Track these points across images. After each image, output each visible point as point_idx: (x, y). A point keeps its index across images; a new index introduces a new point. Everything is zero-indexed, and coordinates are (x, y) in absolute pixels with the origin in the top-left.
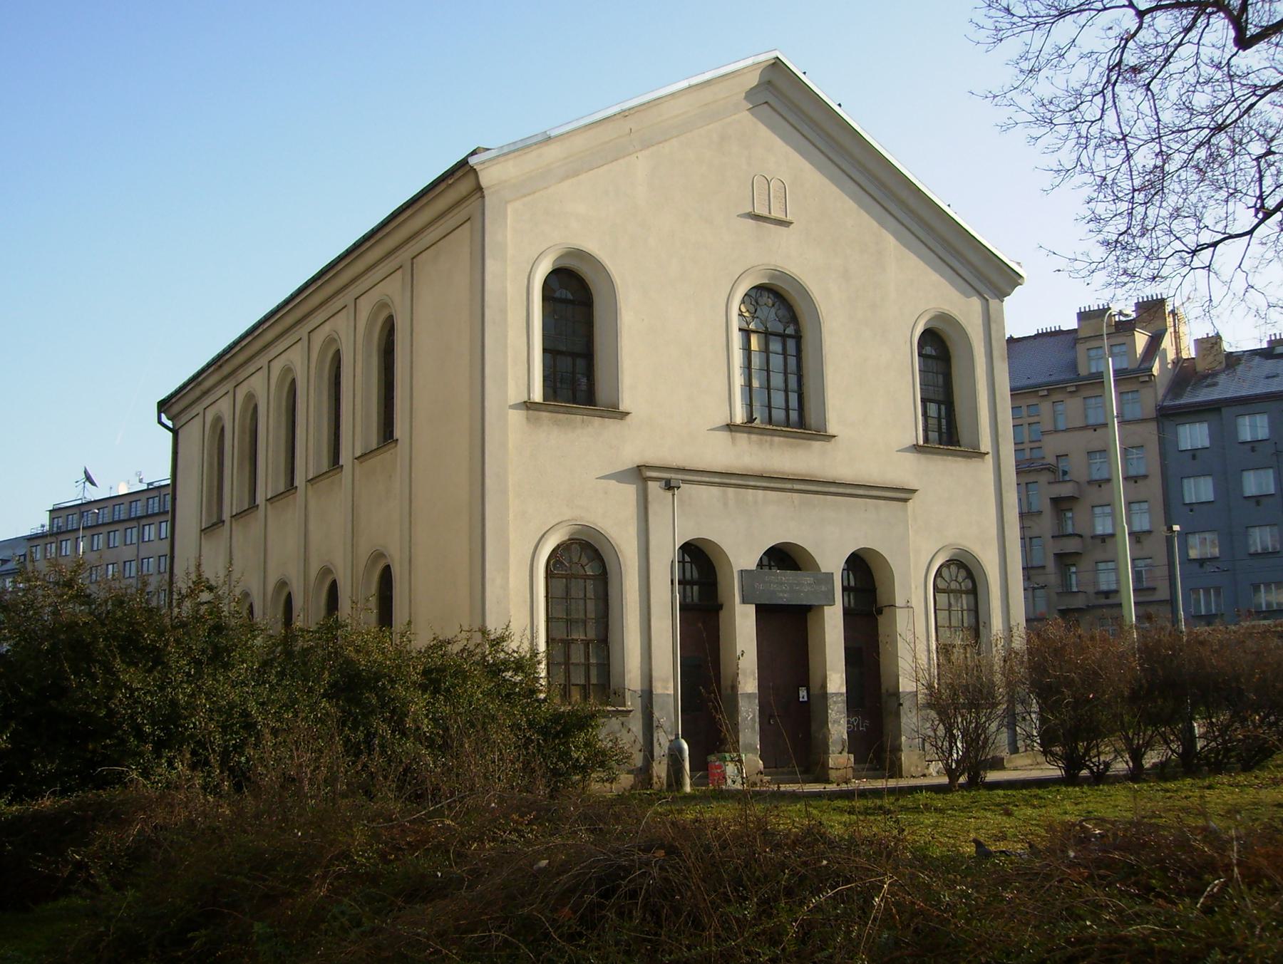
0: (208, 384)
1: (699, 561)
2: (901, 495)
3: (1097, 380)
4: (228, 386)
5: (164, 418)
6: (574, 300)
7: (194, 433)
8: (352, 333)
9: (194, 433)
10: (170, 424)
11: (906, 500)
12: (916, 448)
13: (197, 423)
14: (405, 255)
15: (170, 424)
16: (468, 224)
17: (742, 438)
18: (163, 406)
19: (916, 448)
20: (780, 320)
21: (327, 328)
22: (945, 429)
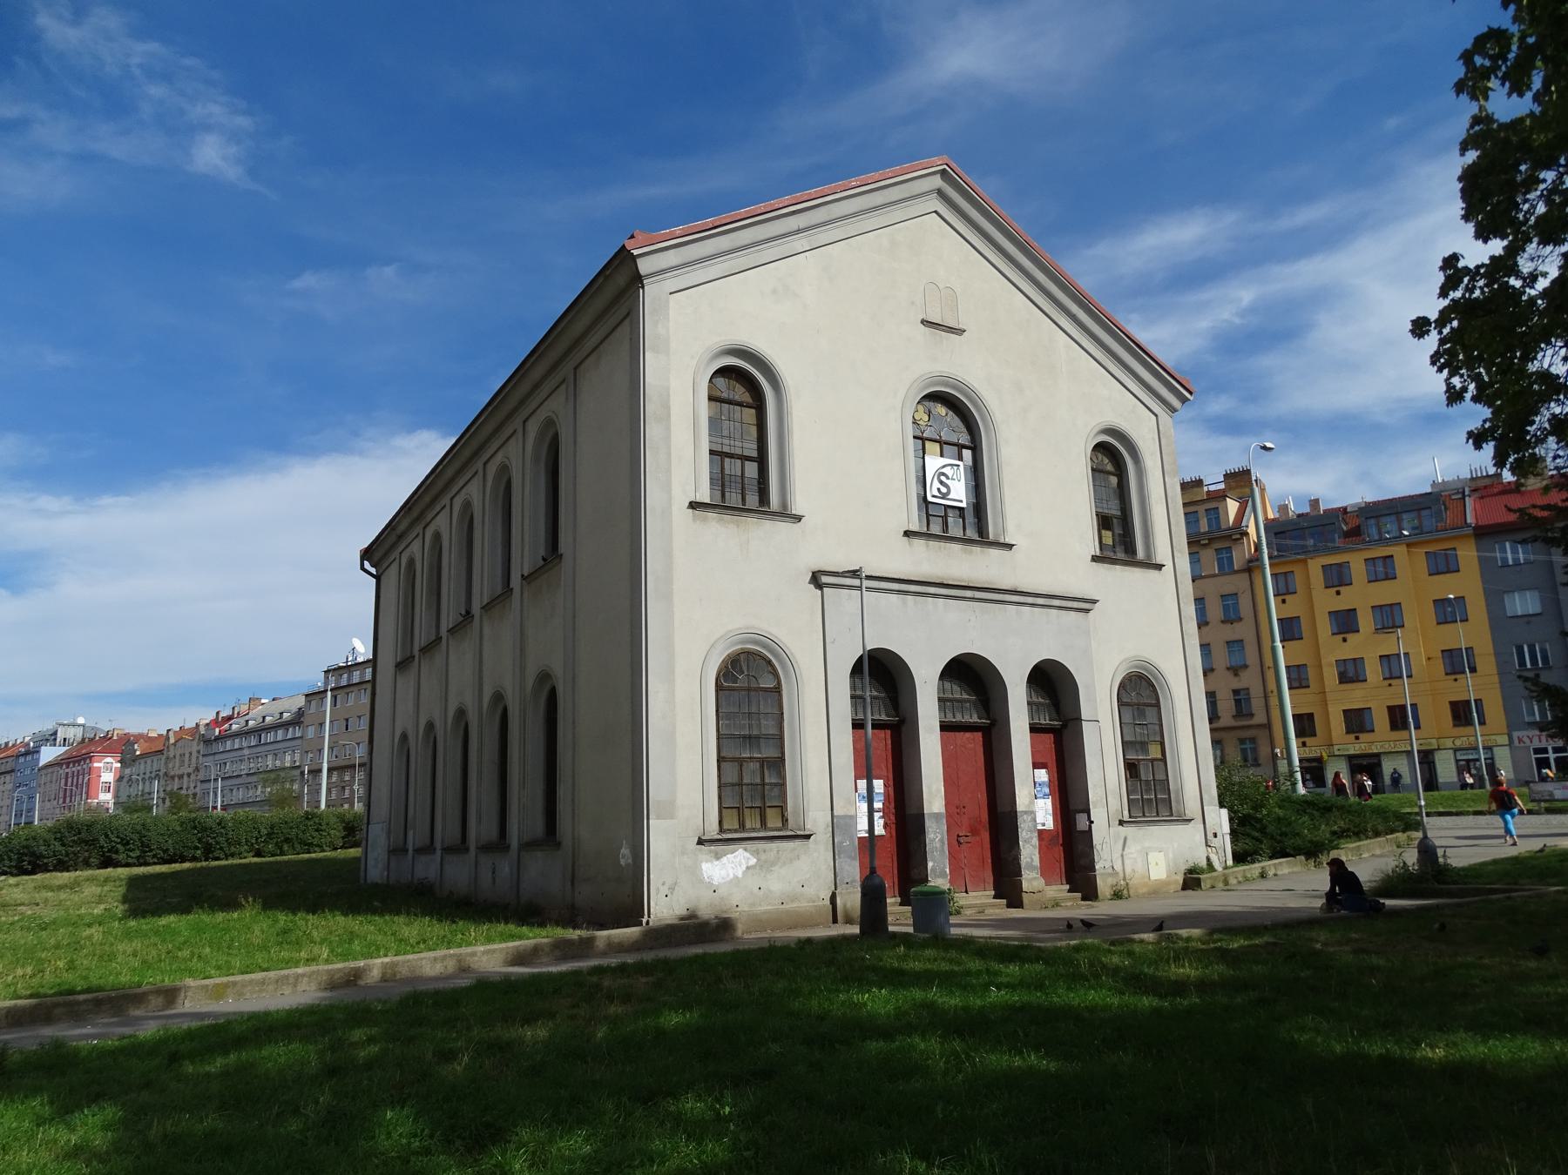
0: (402, 527)
1: (881, 674)
2: (1084, 605)
3: (874, 726)
4: (418, 529)
5: (367, 565)
6: (743, 385)
7: (392, 576)
8: (518, 454)
9: (392, 576)
10: (373, 571)
11: (1087, 611)
12: (1095, 559)
13: (394, 567)
14: (567, 369)
15: (373, 571)
16: (627, 322)
17: (919, 543)
18: (367, 554)
19: (1095, 559)
20: (953, 415)
21: (499, 458)
22: (1119, 537)
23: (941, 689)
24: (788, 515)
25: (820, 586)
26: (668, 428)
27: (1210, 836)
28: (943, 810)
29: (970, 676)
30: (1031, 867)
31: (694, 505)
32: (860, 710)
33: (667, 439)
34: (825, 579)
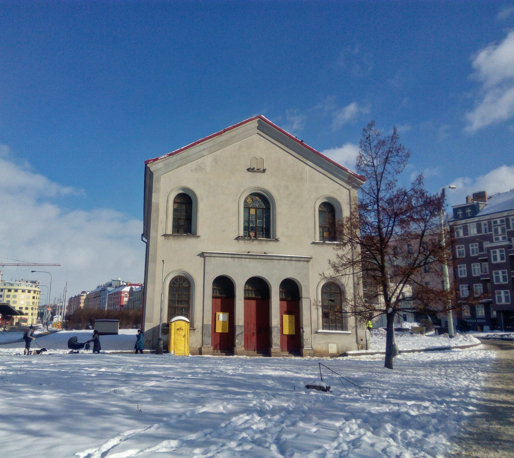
2: (308, 260)
6: (186, 203)
11: (308, 261)
17: (241, 242)
19: (238, 238)
23: (245, 287)
24: (277, 240)
25: (204, 257)
26: (158, 214)
27: (359, 339)
28: (243, 324)
29: (258, 287)
30: (276, 345)
31: (165, 235)
32: (215, 292)
33: (158, 217)
34: (205, 255)
